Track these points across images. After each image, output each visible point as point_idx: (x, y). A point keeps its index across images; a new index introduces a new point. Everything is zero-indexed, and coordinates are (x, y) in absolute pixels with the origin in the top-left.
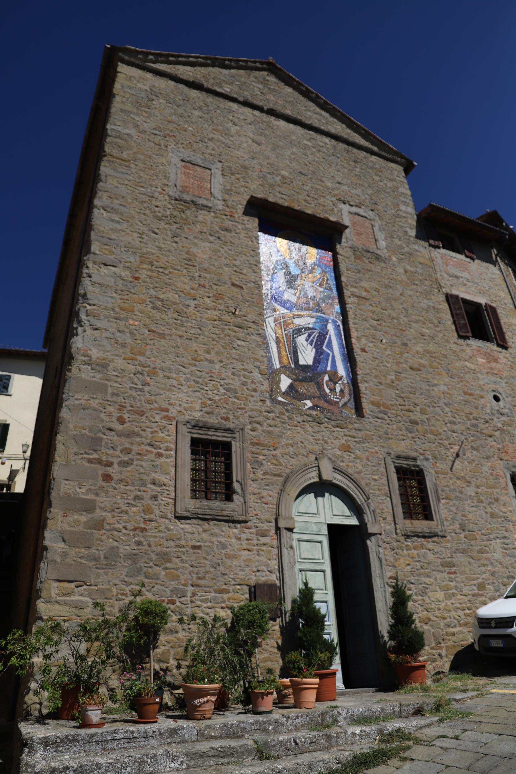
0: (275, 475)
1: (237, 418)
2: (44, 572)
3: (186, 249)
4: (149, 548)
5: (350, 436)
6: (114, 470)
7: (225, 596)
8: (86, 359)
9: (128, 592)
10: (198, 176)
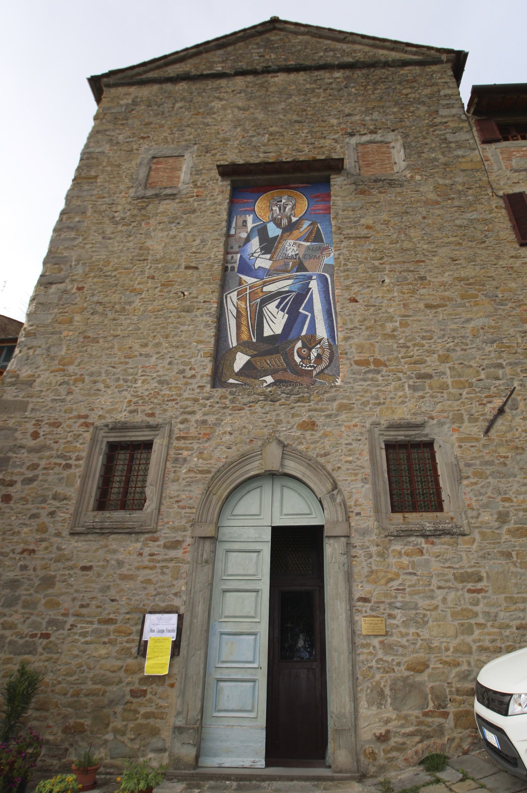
0: (201, 472)
6: (15, 491)
7: (112, 627)
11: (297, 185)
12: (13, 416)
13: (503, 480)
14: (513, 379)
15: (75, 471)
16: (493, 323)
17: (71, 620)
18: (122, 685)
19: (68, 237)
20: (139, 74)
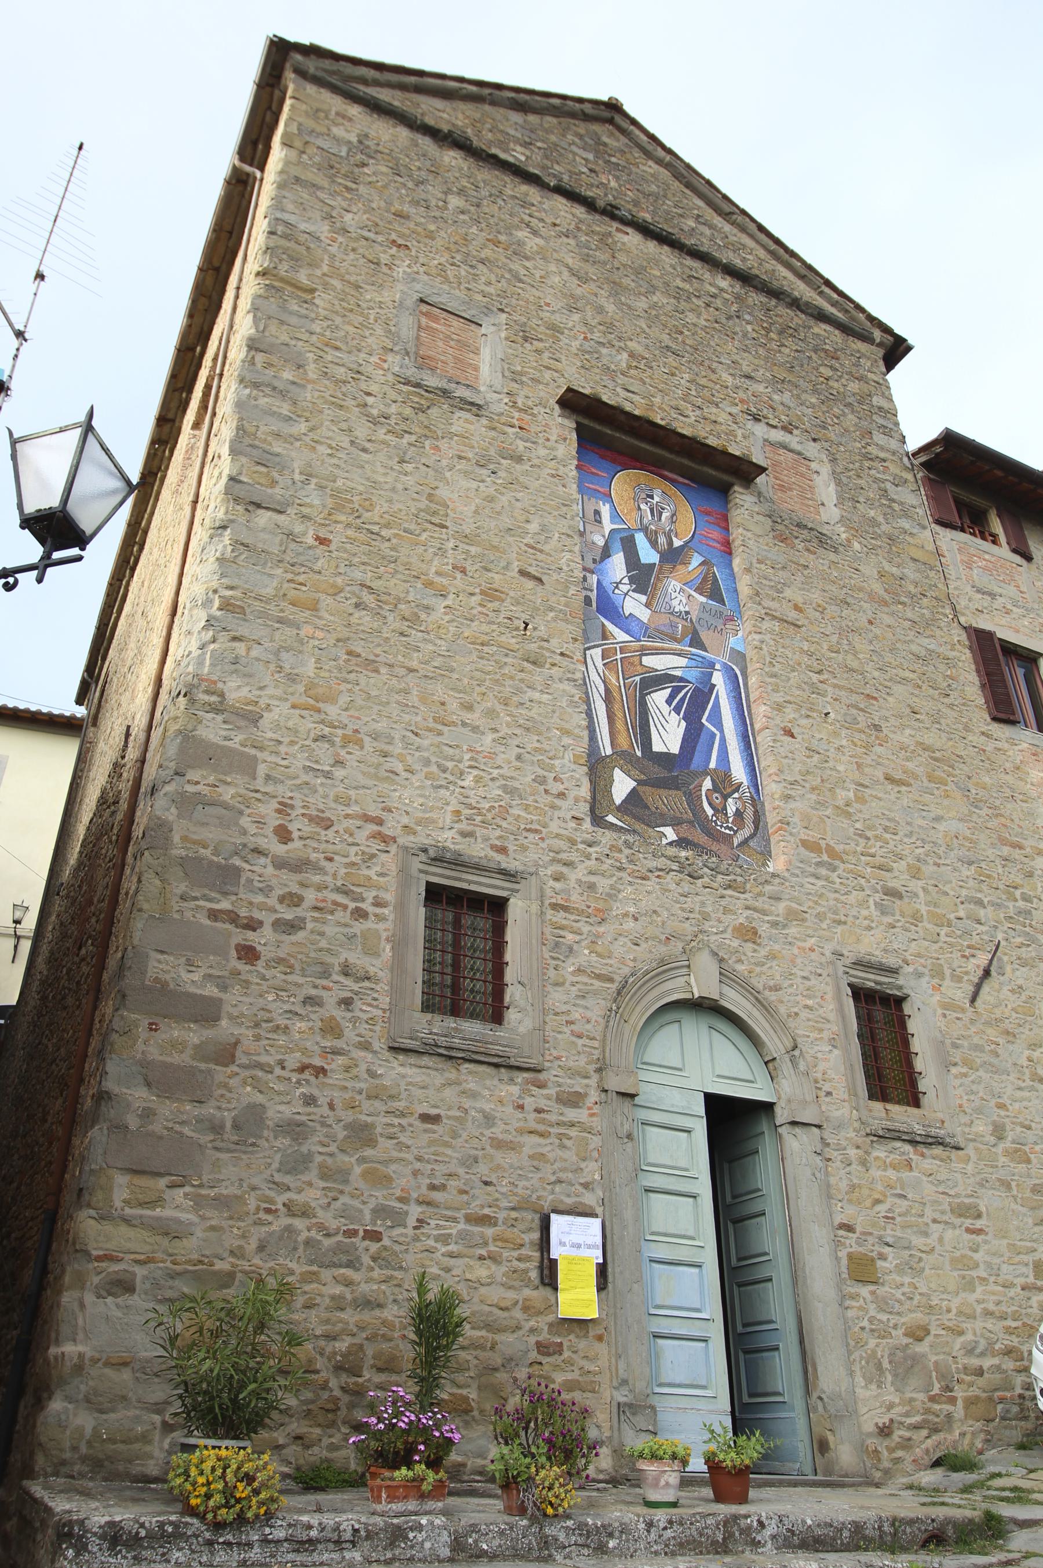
0: (599, 977)
1: (524, 848)
2: (100, 1151)
3: (428, 491)
4: (331, 1113)
5: (755, 910)
6: (264, 939)
7: (489, 1232)
8: (214, 699)
9: (280, 1206)
10: (455, 337)
11: (675, 477)
12: (229, 780)
13: (996, 1077)
14: (996, 927)
15: (375, 926)
16: (968, 833)
17: (415, 1211)
18: (521, 1333)
19: (275, 409)
20: (365, 82)
